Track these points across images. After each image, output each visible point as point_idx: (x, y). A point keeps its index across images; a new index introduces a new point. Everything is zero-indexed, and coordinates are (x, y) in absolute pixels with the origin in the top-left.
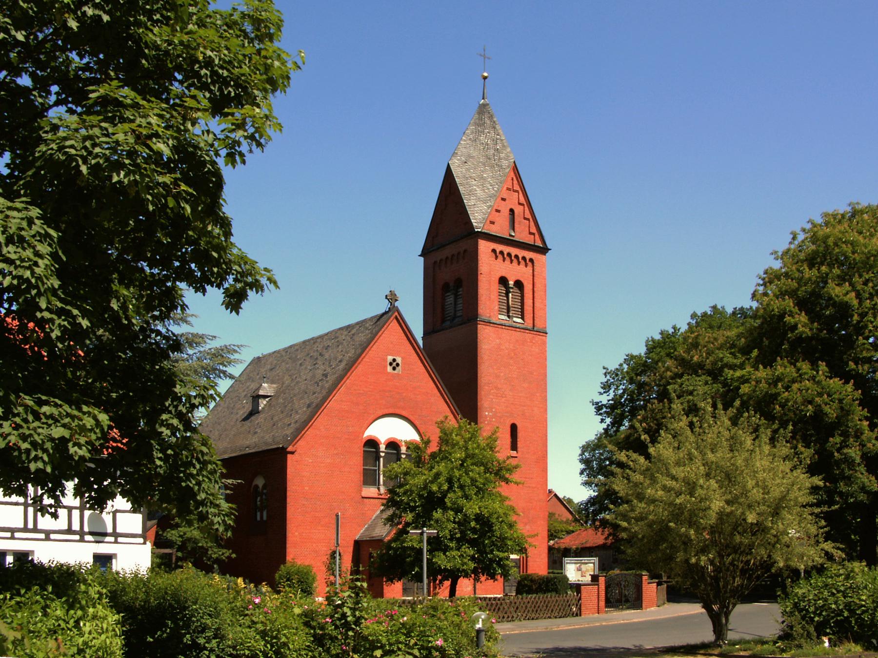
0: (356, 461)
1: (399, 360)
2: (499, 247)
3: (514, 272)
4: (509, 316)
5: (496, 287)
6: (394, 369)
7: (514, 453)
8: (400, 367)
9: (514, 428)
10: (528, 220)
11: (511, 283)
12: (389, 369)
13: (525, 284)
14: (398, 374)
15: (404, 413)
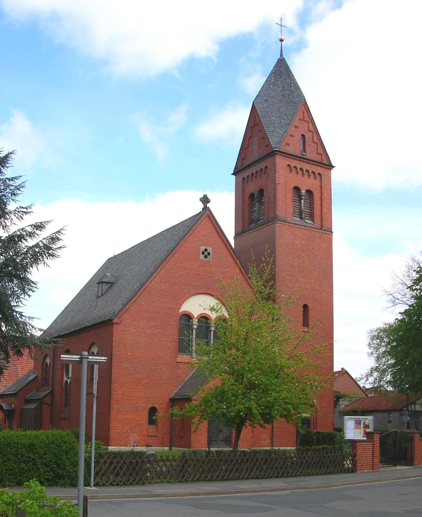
0: (172, 332)
1: (210, 250)
2: (294, 163)
3: (306, 183)
4: (301, 218)
5: (290, 194)
6: (206, 257)
7: (305, 329)
8: (211, 256)
9: (305, 307)
10: (317, 144)
11: (303, 192)
12: (202, 257)
13: (315, 193)
14: (209, 262)
15: (213, 293)
